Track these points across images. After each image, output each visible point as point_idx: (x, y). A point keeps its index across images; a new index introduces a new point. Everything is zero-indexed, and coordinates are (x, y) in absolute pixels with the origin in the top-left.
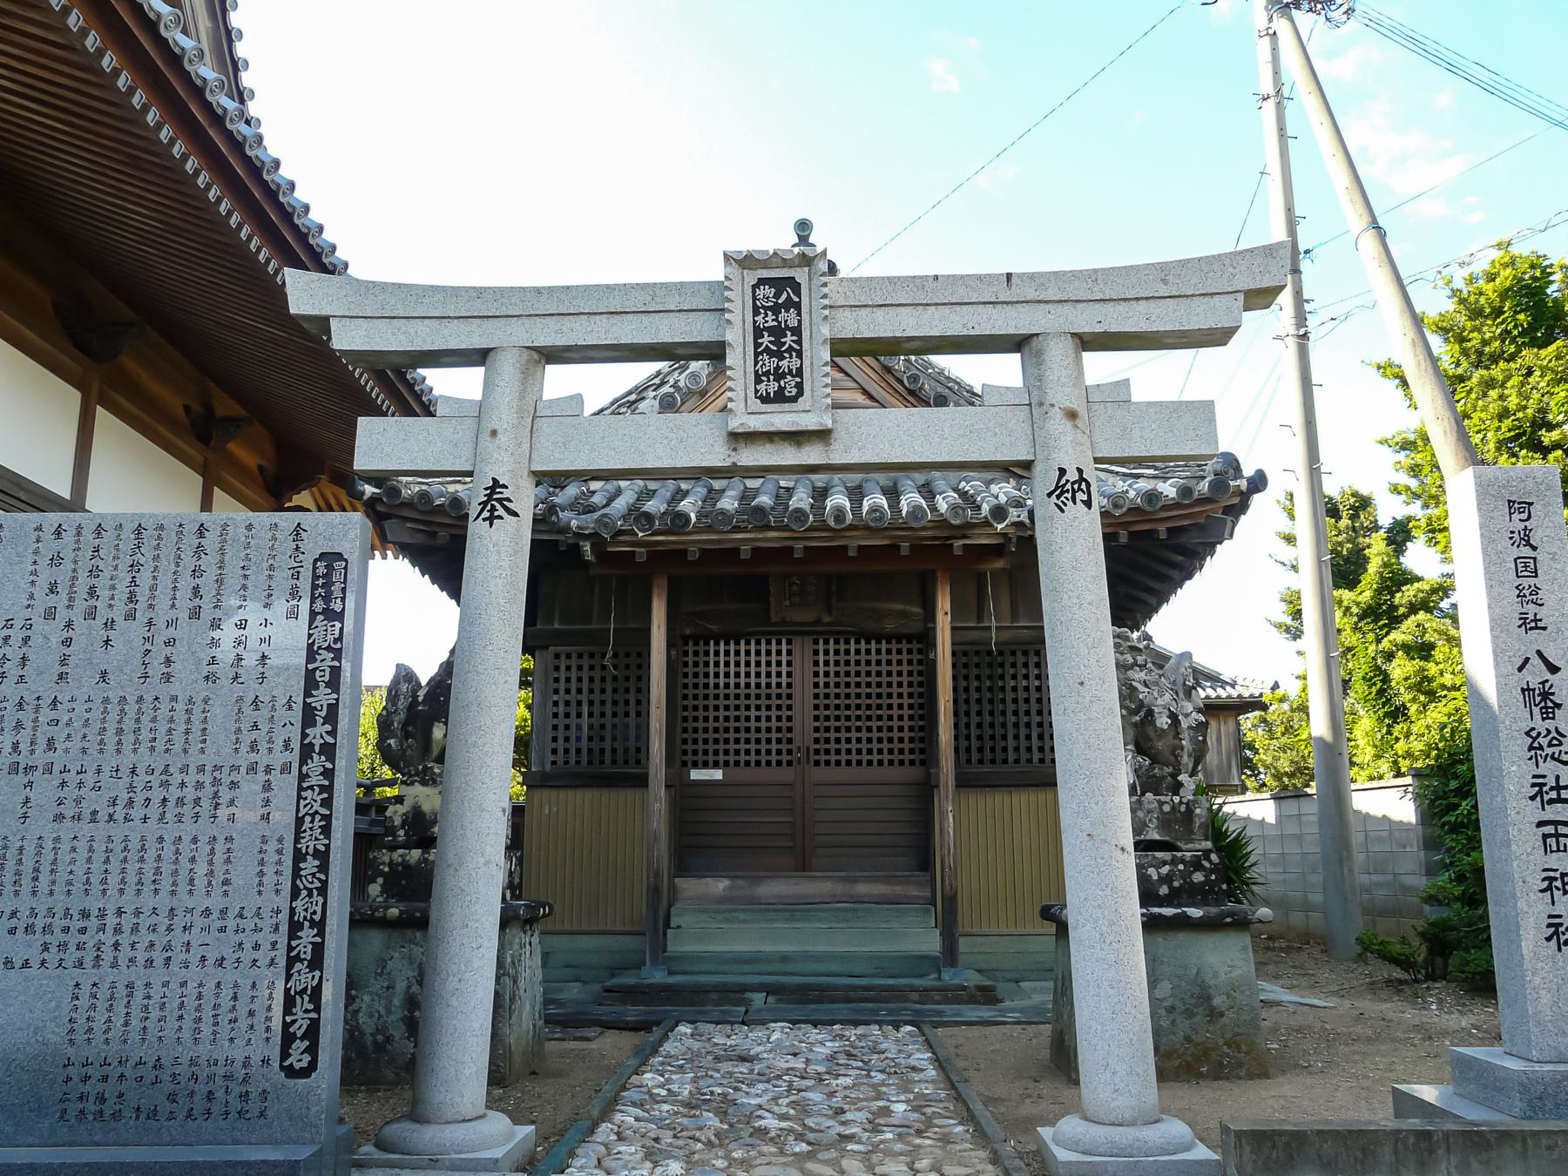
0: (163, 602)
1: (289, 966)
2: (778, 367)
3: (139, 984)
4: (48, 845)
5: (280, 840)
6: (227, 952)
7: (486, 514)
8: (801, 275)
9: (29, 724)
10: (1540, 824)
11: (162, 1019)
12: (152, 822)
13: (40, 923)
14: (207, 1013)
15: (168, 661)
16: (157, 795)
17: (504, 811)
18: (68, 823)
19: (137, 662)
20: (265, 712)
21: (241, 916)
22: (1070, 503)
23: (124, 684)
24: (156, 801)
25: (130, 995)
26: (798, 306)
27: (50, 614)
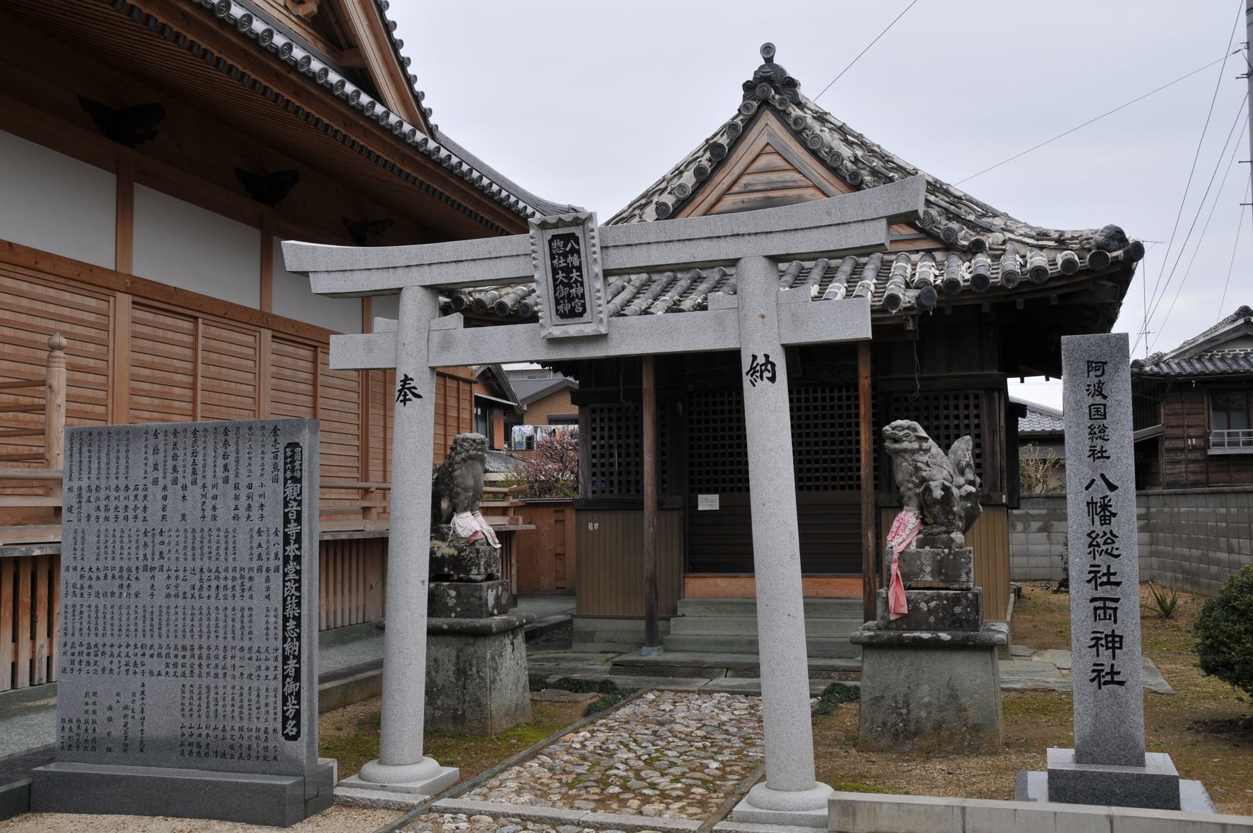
0: (210, 474)
1: (284, 680)
2: (570, 294)
3: (212, 686)
4: (165, 610)
5: (276, 610)
6: (253, 671)
7: (401, 398)
8: (578, 231)
9: (150, 544)
10: (1093, 600)
11: (224, 706)
12: (213, 598)
13: (164, 652)
14: (246, 704)
15: (214, 508)
16: (214, 584)
17: (423, 582)
18: (173, 599)
19: (199, 509)
20: (264, 537)
21: (258, 651)
22: (759, 380)
23: (194, 521)
24: (213, 587)
25: (209, 692)
26: (578, 252)
27: (155, 482)
